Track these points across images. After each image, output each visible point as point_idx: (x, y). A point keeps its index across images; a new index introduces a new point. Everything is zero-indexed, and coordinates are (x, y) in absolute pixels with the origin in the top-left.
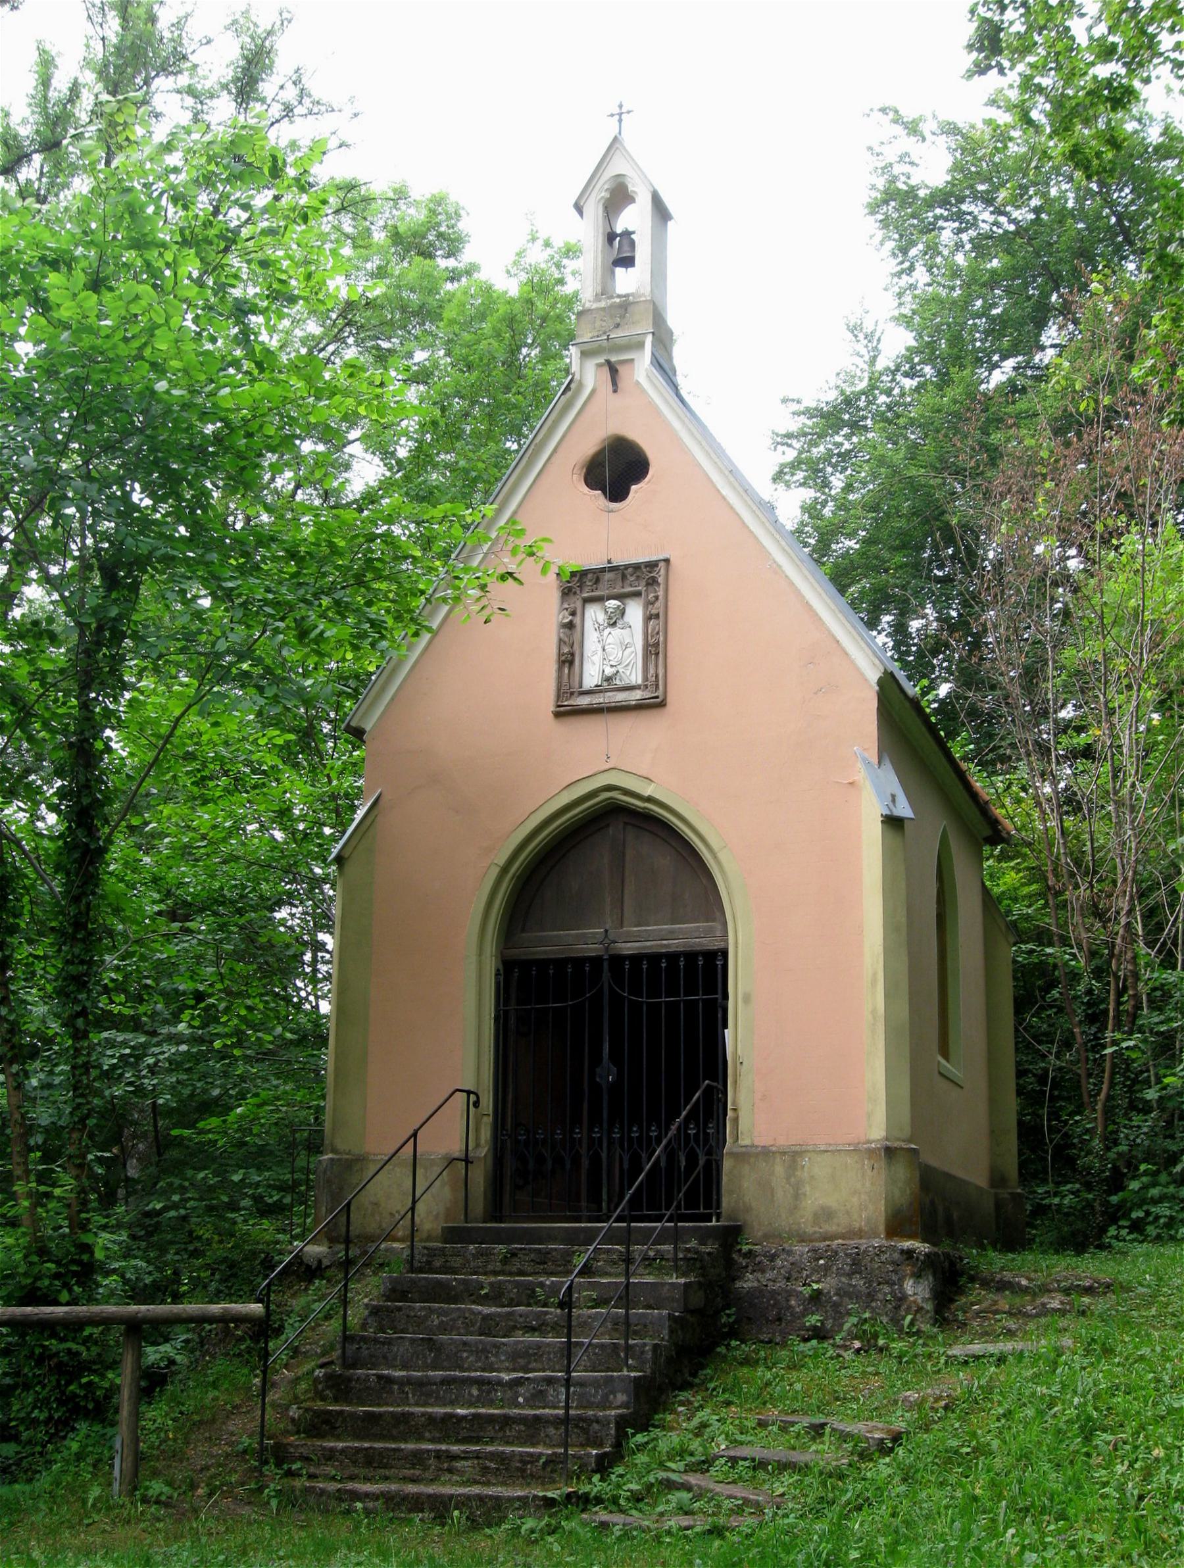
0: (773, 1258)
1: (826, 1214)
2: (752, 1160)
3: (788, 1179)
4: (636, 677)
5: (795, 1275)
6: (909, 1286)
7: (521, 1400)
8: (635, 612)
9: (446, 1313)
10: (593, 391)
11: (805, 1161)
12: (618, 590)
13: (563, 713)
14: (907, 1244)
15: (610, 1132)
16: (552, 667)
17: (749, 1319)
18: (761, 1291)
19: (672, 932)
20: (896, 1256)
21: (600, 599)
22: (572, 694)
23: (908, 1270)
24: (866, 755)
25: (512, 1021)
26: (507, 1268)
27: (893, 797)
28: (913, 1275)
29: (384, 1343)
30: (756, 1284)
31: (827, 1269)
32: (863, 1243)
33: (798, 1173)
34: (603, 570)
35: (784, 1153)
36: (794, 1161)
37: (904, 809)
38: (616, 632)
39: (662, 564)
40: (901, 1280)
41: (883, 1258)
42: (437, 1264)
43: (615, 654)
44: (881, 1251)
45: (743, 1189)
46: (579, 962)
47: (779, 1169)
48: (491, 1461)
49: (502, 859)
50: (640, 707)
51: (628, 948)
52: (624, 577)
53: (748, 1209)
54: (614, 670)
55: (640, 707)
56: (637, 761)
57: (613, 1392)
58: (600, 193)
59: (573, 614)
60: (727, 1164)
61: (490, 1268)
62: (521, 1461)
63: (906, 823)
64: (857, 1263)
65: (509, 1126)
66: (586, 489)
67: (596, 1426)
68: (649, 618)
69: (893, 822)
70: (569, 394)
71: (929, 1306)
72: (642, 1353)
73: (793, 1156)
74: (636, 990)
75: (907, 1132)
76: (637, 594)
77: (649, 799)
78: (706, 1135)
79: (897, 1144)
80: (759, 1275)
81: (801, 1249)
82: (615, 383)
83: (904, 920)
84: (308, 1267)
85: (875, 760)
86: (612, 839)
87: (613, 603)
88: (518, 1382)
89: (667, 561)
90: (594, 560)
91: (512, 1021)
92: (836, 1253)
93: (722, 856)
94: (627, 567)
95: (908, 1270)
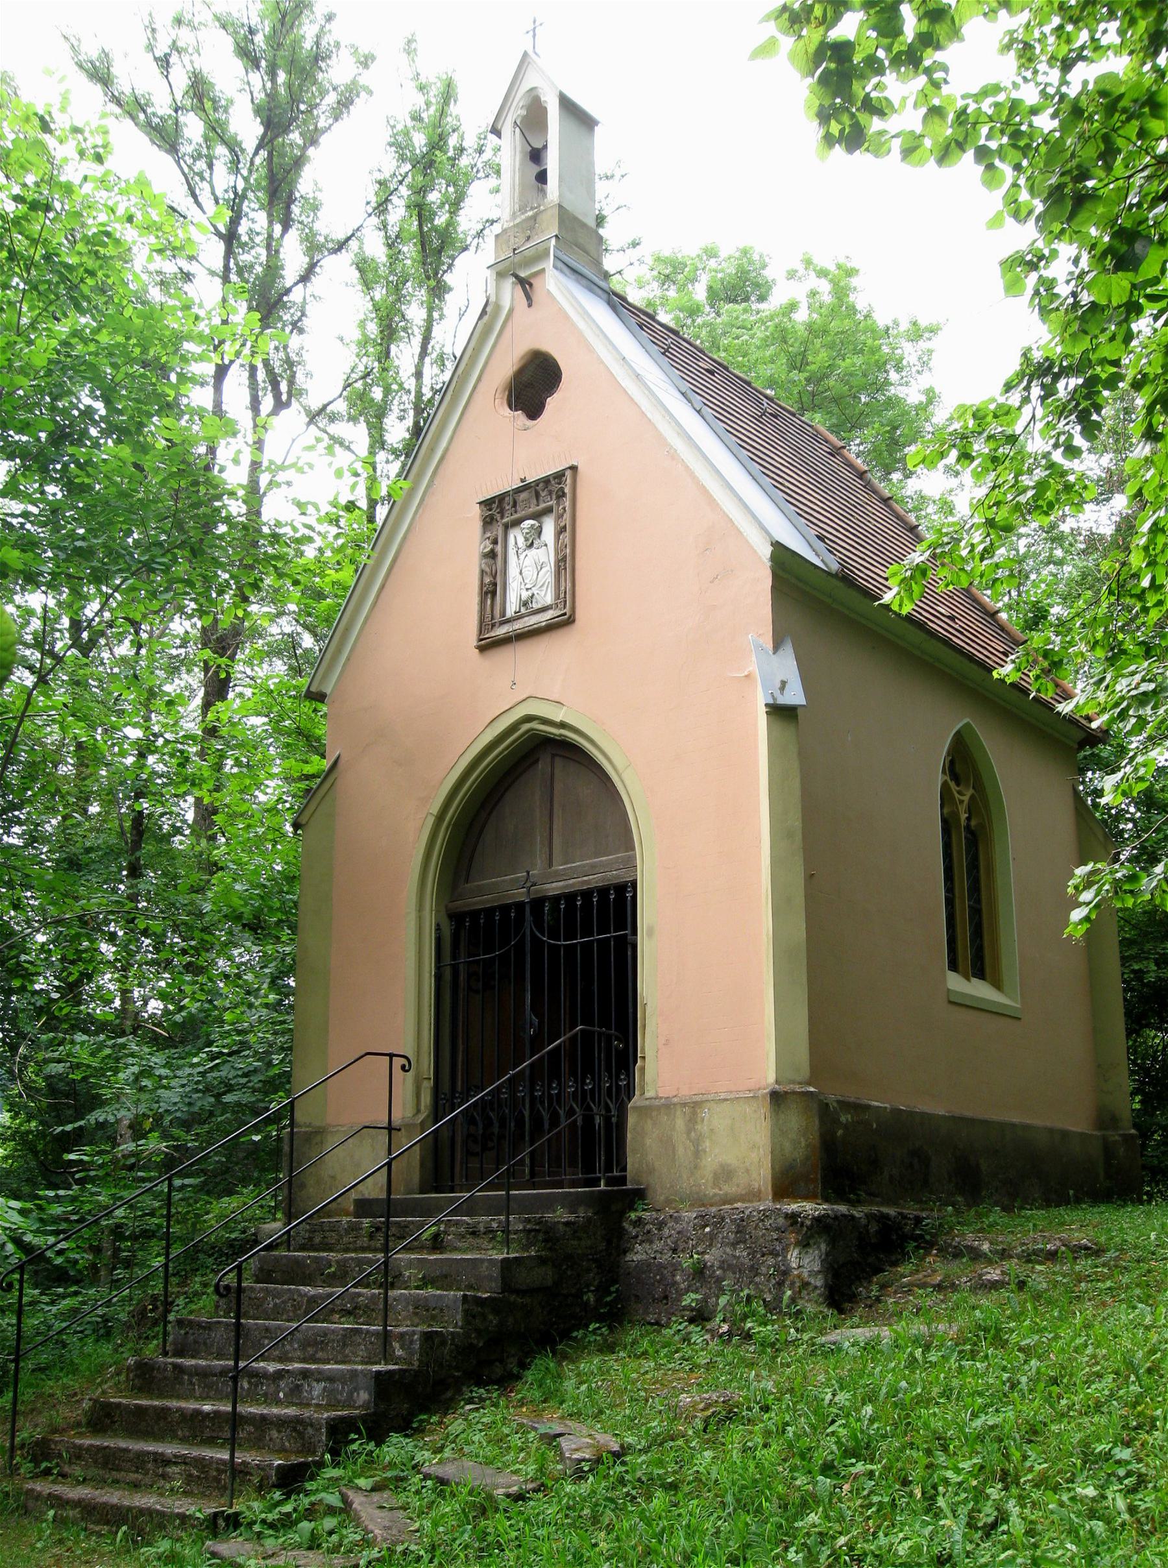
0: (661, 1225)
1: (725, 1173)
2: (654, 1114)
3: (688, 1132)
4: (548, 598)
5: (681, 1245)
6: (793, 1257)
7: (281, 1395)
8: (549, 527)
9: (277, 1295)
10: (511, 310)
11: (705, 1113)
12: (533, 509)
13: (487, 646)
14: (794, 1207)
15: (532, 1090)
16: (475, 599)
17: (637, 1296)
18: (649, 1265)
19: (593, 866)
20: (781, 1221)
21: (517, 523)
22: (493, 625)
23: (792, 1238)
24: (761, 641)
25: (462, 977)
26: (373, 1243)
27: (784, 683)
28: (798, 1243)
29: (204, 1328)
30: (644, 1257)
31: (712, 1237)
32: (747, 1207)
33: (698, 1127)
34: (518, 491)
35: (684, 1105)
36: (694, 1113)
37: (795, 696)
38: (532, 552)
39: (568, 473)
40: (785, 1249)
41: (767, 1223)
42: (317, 1240)
43: (530, 573)
44: (765, 1215)
45: (650, 1148)
46: (505, 909)
47: (680, 1123)
48: (195, 1467)
49: (435, 808)
50: (550, 628)
51: (554, 888)
52: (537, 496)
53: (651, 1171)
54: (530, 593)
55: (550, 628)
56: (550, 686)
57: (356, 1389)
58: (516, 112)
59: (495, 542)
60: (631, 1120)
61: (359, 1243)
62: (218, 1470)
63: (799, 711)
64: (741, 1227)
65: (459, 1089)
66: (507, 411)
67: (310, 1430)
68: (560, 531)
69: (780, 712)
70: (486, 318)
71: (819, 1282)
72: (412, 1342)
73: (694, 1107)
74: (554, 935)
75: (805, 1072)
76: (549, 510)
77: (563, 725)
78: (618, 1087)
79: (788, 1088)
80: (647, 1246)
81: (689, 1215)
82: (529, 298)
83: (798, 824)
84: (832, 1243)
85: (770, 646)
86: (536, 769)
87: (528, 523)
88: (279, 1375)
89: (574, 468)
90: (506, 483)
91: (462, 977)
92: (723, 1219)
93: (625, 776)
94: (537, 482)
95: (792, 1238)
